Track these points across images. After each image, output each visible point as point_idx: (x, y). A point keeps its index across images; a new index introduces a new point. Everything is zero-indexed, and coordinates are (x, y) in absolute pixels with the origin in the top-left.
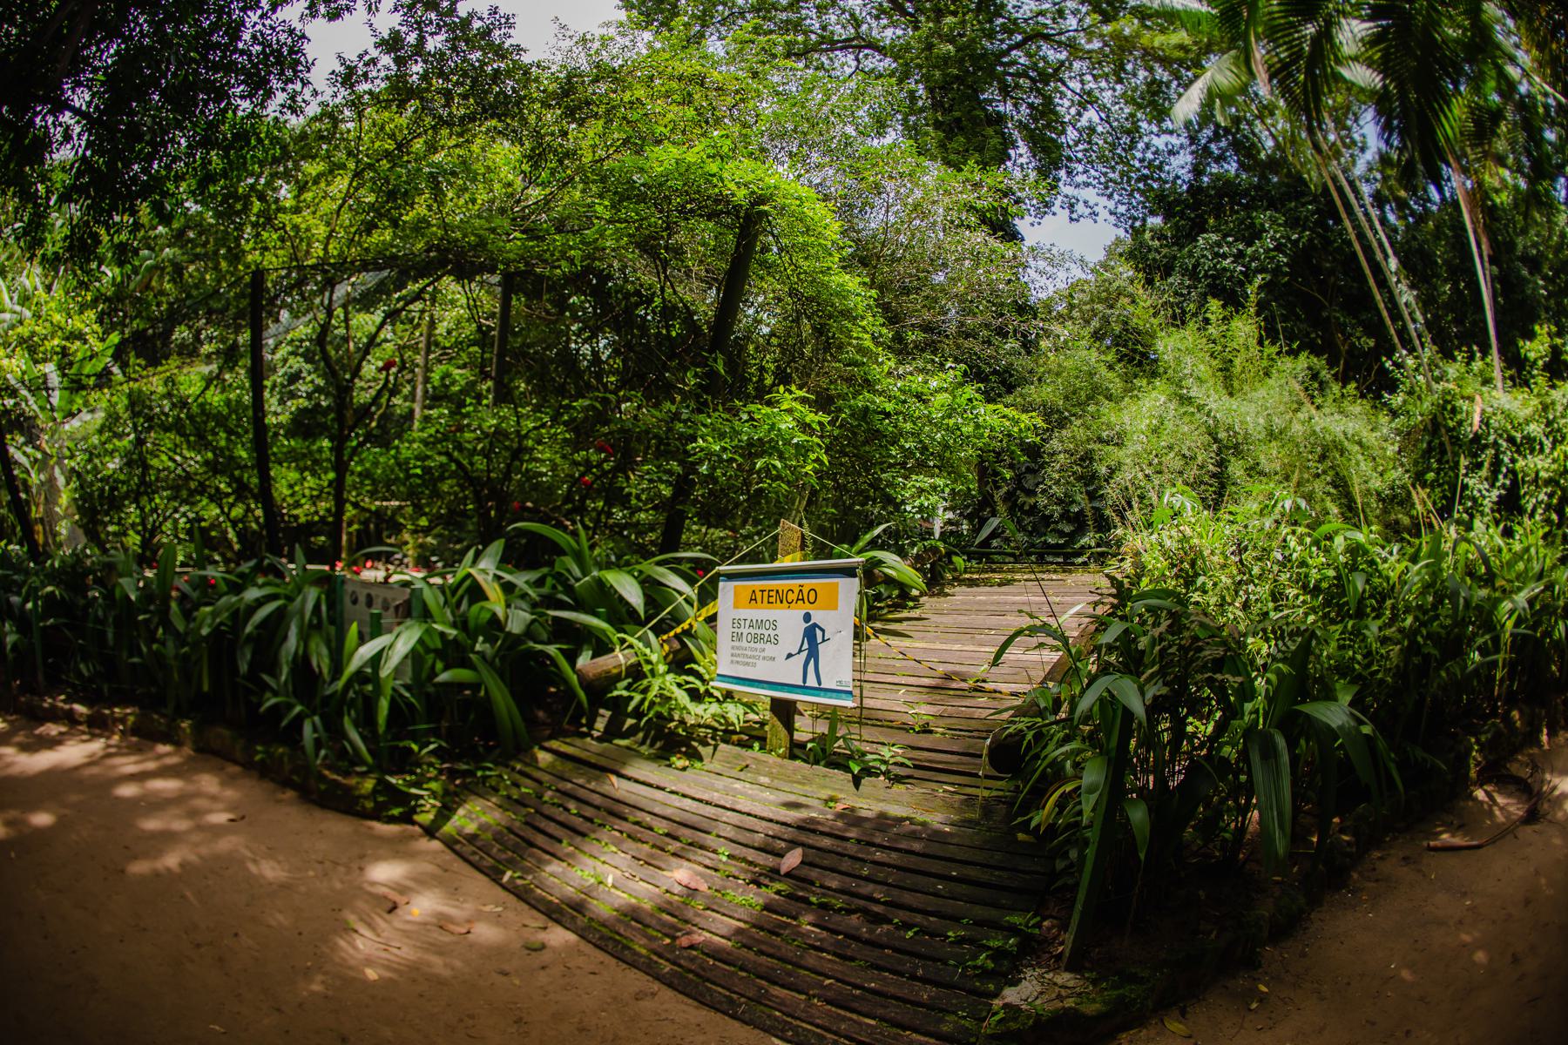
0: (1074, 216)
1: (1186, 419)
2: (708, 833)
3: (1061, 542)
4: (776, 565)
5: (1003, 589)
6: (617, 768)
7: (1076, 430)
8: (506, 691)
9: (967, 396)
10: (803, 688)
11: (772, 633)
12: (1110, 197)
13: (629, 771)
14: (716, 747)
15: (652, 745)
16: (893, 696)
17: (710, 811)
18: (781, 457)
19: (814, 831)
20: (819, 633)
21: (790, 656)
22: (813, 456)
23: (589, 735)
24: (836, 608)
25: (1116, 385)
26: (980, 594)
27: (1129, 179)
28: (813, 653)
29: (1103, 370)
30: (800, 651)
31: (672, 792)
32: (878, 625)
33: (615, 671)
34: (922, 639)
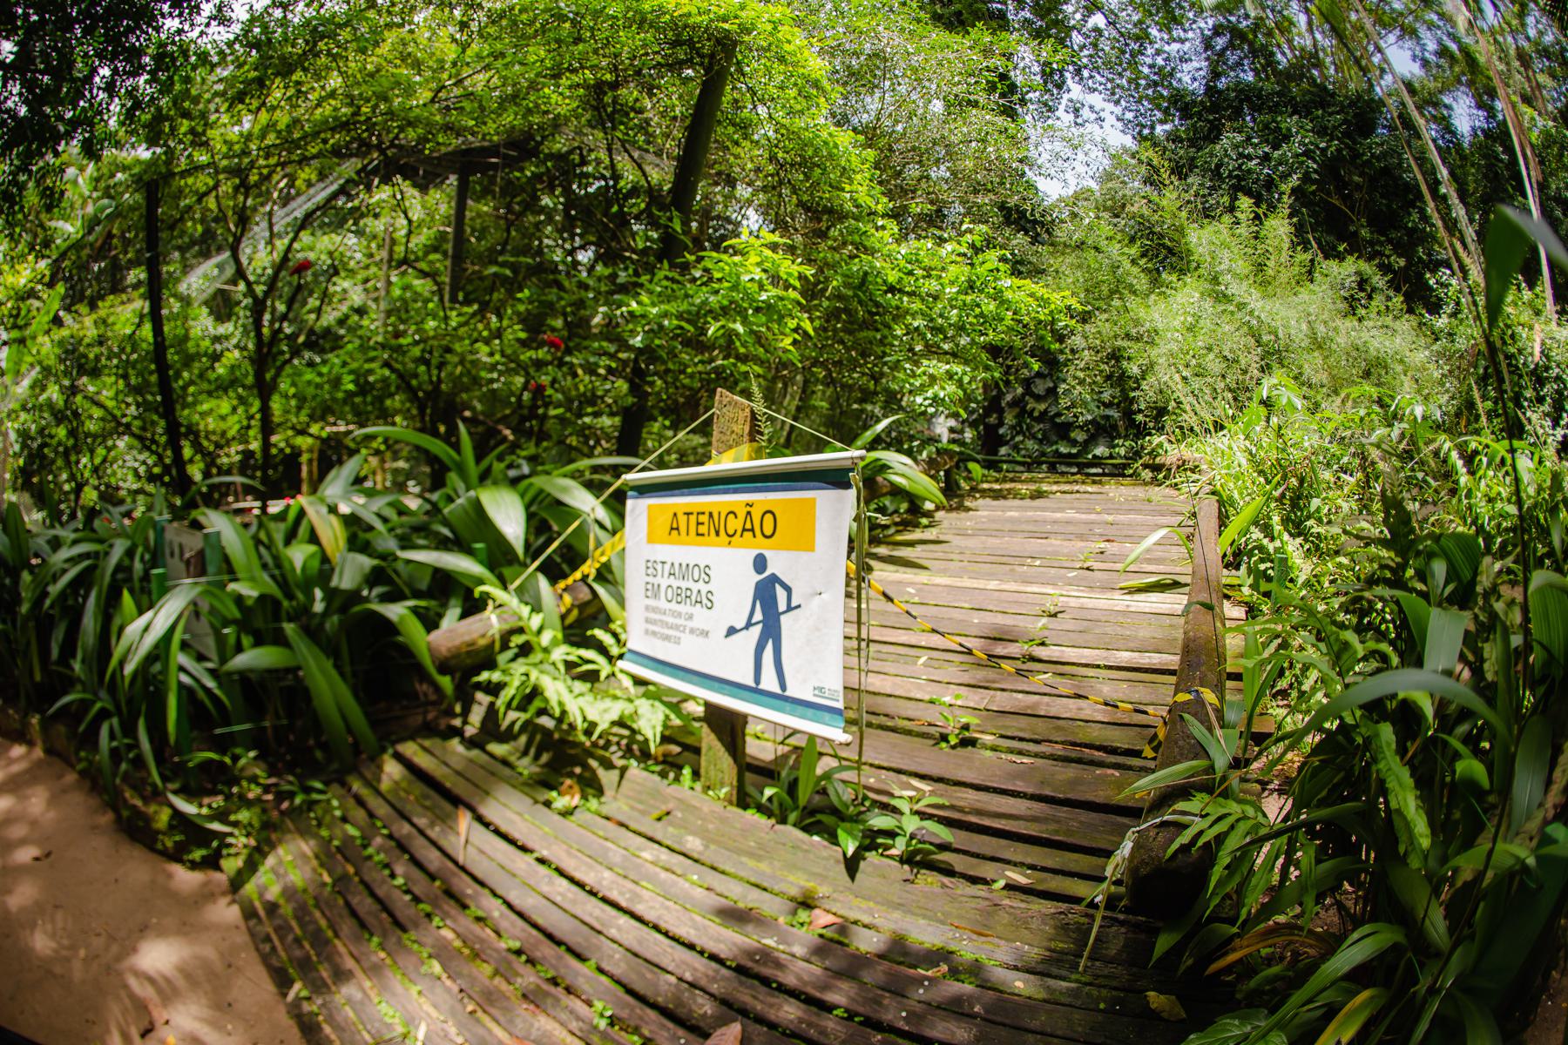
0: (1079, 121)
1: (1226, 318)
2: (581, 958)
3: (1074, 451)
4: (709, 468)
5: (1038, 502)
6: (474, 801)
7: (1102, 325)
8: (329, 664)
9: (989, 266)
10: (754, 692)
11: (704, 588)
12: (1117, 103)
13: (490, 811)
14: (623, 770)
15: (537, 757)
16: (908, 670)
17: (593, 910)
18: (745, 322)
19: (765, 981)
20: (781, 594)
21: (732, 631)
22: (792, 324)
23: (458, 732)
24: (810, 547)
25: (1142, 282)
26: (1011, 509)
27: (1138, 85)
28: (771, 631)
29: (1127, 264)
30: (749, 625)
31: (541, 861)
32: (882, 550)
33: (482, 642)
34: (944, 572)
